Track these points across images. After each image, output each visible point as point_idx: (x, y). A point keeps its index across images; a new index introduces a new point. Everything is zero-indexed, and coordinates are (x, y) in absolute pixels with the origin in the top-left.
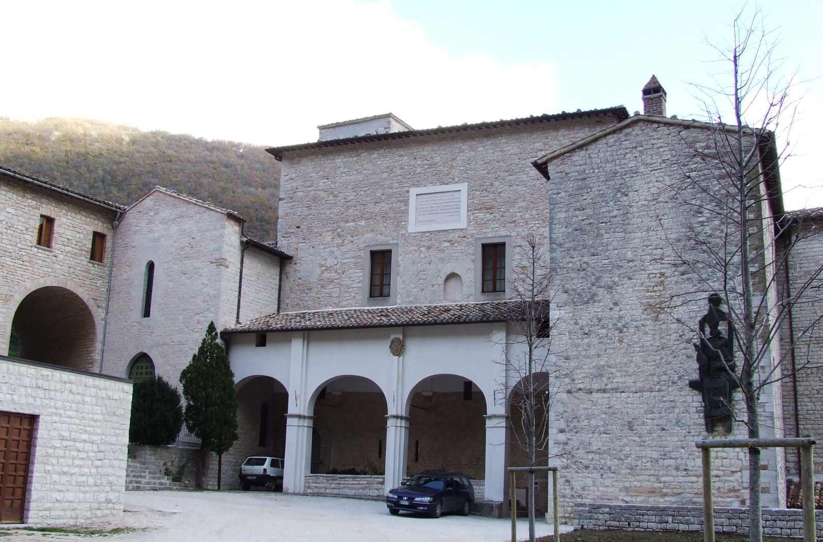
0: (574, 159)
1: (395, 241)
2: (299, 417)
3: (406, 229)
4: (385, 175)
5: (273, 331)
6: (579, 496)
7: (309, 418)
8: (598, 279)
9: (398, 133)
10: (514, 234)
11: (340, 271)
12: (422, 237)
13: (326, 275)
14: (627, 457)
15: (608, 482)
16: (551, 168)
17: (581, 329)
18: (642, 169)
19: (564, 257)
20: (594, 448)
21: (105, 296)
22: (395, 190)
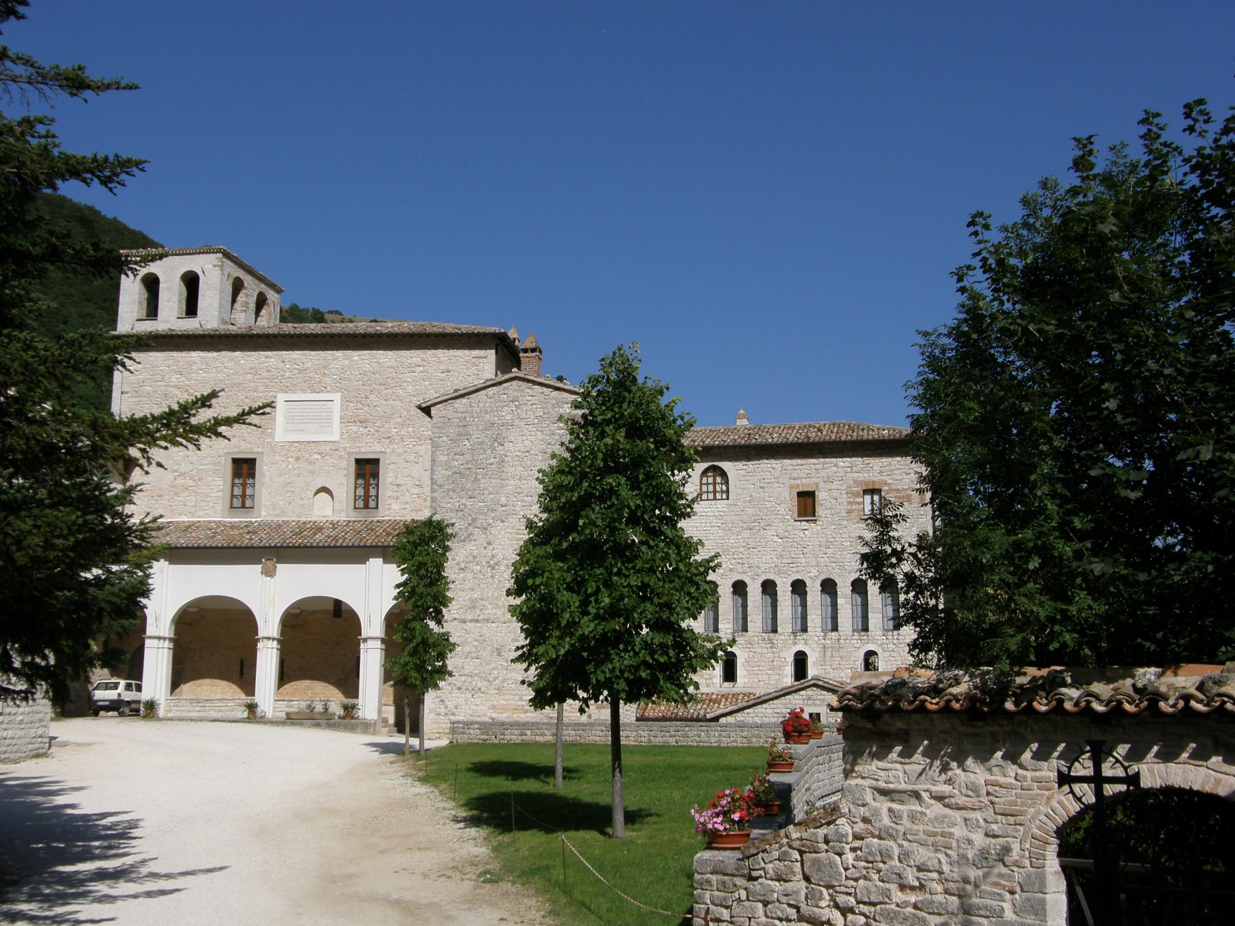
0: (457, 406)
1: (260, 450)
2: (159, 638)
3: (273, 437)
4: (249, 377)
6: (452, 714)
8: (474, 520)
9: (525, 794)
10: (388, 451)
11: (197, 478)
12: (290, 447)
13: (180, 481)
14: (495, 679)
15: (478, 701)
16: (433, 411)
17: (458, 564)
18: (517, 422)
19: (443, 498)
20: (467, 672)
22: (260, 395)
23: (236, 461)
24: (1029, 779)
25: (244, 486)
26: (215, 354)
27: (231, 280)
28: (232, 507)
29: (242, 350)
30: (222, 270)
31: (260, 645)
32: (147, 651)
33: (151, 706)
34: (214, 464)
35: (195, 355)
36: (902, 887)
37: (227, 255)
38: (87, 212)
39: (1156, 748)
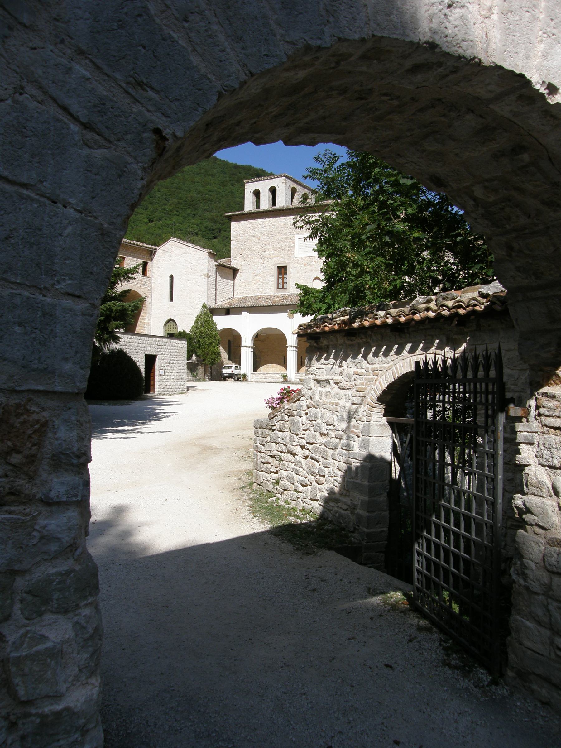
2: (247, 347)
5: (233, 308)
7: (252, 347)
13: (256, 278)
21: (407, 472)
23: (279, 268)
24: (370, 370)
25: (283, 278)
26: (268, 220)
27: (290, 189)
28: (278, 288)
29: (279, 216)
30: (286, 184)
31: (288, 349)
32: (242, 353)
33: (244, 376)
34: (270, 269)
35: (260, 221)
36: (322, 434)
37: (287, 177)
38: (260, 171)
39: (422, 345)
